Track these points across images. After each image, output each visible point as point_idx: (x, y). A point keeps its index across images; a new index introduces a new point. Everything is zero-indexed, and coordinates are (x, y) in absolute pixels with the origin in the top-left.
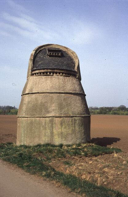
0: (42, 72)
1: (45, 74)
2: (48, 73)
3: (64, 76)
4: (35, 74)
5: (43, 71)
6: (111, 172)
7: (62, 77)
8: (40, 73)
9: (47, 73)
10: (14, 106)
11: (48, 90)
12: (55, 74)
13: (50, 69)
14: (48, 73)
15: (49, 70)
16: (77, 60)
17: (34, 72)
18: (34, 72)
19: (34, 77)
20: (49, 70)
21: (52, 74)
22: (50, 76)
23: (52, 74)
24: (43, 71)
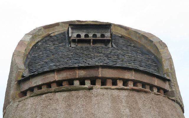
0: (55, 82)
1: (65, 85)
2: (77, 83)
3: (133, 90)
4: (31, 89)
5: (57, 77)
6: (60, 76)
7: (124, 93)
8: (49, 85)
9: (71, 82)
10: (23, 76)
11: (59, 95)
12: (98, 86)
13: (80, 68)
14: (77, 83)
15: (81, 73)
16: (89, 22)
17: (26, 86)
18: (26, 86)
19: (30, 102)
20: (81, 73)
21: (88, 84)
22: (81, 93)
23: (88, 84)
24: (57, 77)
